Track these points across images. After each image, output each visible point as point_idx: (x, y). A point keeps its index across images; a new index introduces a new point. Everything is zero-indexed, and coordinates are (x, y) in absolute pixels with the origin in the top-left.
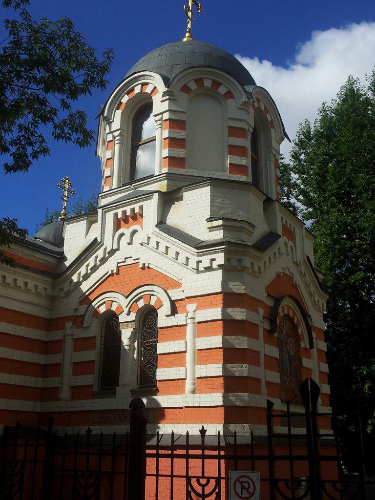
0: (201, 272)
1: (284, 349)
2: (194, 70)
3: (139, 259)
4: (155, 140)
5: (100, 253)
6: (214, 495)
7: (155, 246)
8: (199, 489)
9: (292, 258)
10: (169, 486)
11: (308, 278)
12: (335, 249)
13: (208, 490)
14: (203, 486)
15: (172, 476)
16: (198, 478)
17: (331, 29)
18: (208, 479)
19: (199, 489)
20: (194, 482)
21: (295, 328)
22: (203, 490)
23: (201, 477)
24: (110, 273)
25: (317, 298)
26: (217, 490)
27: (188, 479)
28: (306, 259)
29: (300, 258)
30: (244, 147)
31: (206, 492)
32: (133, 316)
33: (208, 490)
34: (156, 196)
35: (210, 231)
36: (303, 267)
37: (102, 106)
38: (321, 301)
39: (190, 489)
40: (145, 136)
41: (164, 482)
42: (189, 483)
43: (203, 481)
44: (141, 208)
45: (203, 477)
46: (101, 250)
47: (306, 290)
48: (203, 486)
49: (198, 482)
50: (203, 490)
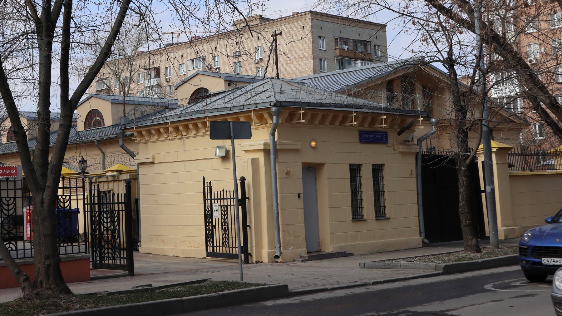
3: (380, 214)
6: (13, 205)
8: (6, 203)
12: (449, 23)
13: (10, 203)
14: (8, 201)
15: (24, 249)
16: (5, 198)
17: (421, 284)
18: (10, 198)
19: (6, 203)
20: (14, 248)
22: (8, 203)
23: (7, 198)
26: (14, 202)
30: (333, 116)
31: (9, 204)
33: (10, 203)
37: (351, 119)
39: (2, 203)
42: (16, 248)
43: (8, 199)
45: (8, 197)
48: (8, 201)
49: (6, 199)
50: (8, 203)
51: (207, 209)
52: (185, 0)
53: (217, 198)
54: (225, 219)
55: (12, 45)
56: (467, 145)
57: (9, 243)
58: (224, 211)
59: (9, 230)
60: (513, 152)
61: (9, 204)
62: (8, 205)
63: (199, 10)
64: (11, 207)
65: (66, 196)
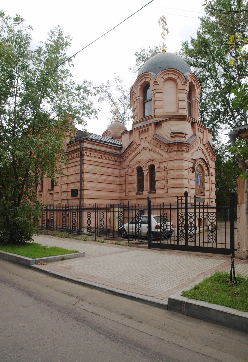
0: (168, 153)
1: (198, 177)
2: (165, 71)
4: (152, 100)
5: (135, 146)
6: (209, 239)
7: (153, 143)
8: (213, 240)
9: (203, 143)
10: (86, 190)
11: (209, 150)
13: (211, 240)
19: (213, 240)
20: (215, 242)
21: (202, 169)
24: (139, 153)
25: (212, 157)
27: (216, 243)
28: (208, 143)
29: (205, 143)
31: (211, 239)
32: (147, 168)
33: (211, 240)
34: (153, 125)
35: (171, 138)
36: (207, 146)
38: (214, 158)
40: (148, 98)
41: (223, 242)
42: (136, 214)
44: (148, 129)
46: (135, 145)
47: (208, 154)
51: (88, 214)
52: (1, 14)
53: (127, 219)
54: (44, 216)
55: (14, 132)
56: (94, 141)
57: (164, 217)
58: (74, 214)
59: (212, 225)
60: (5, 258)
61: (211, 239)
62: (212, 239)
63: (138, 330)
64: (211, 237)
65: (211, 242)
